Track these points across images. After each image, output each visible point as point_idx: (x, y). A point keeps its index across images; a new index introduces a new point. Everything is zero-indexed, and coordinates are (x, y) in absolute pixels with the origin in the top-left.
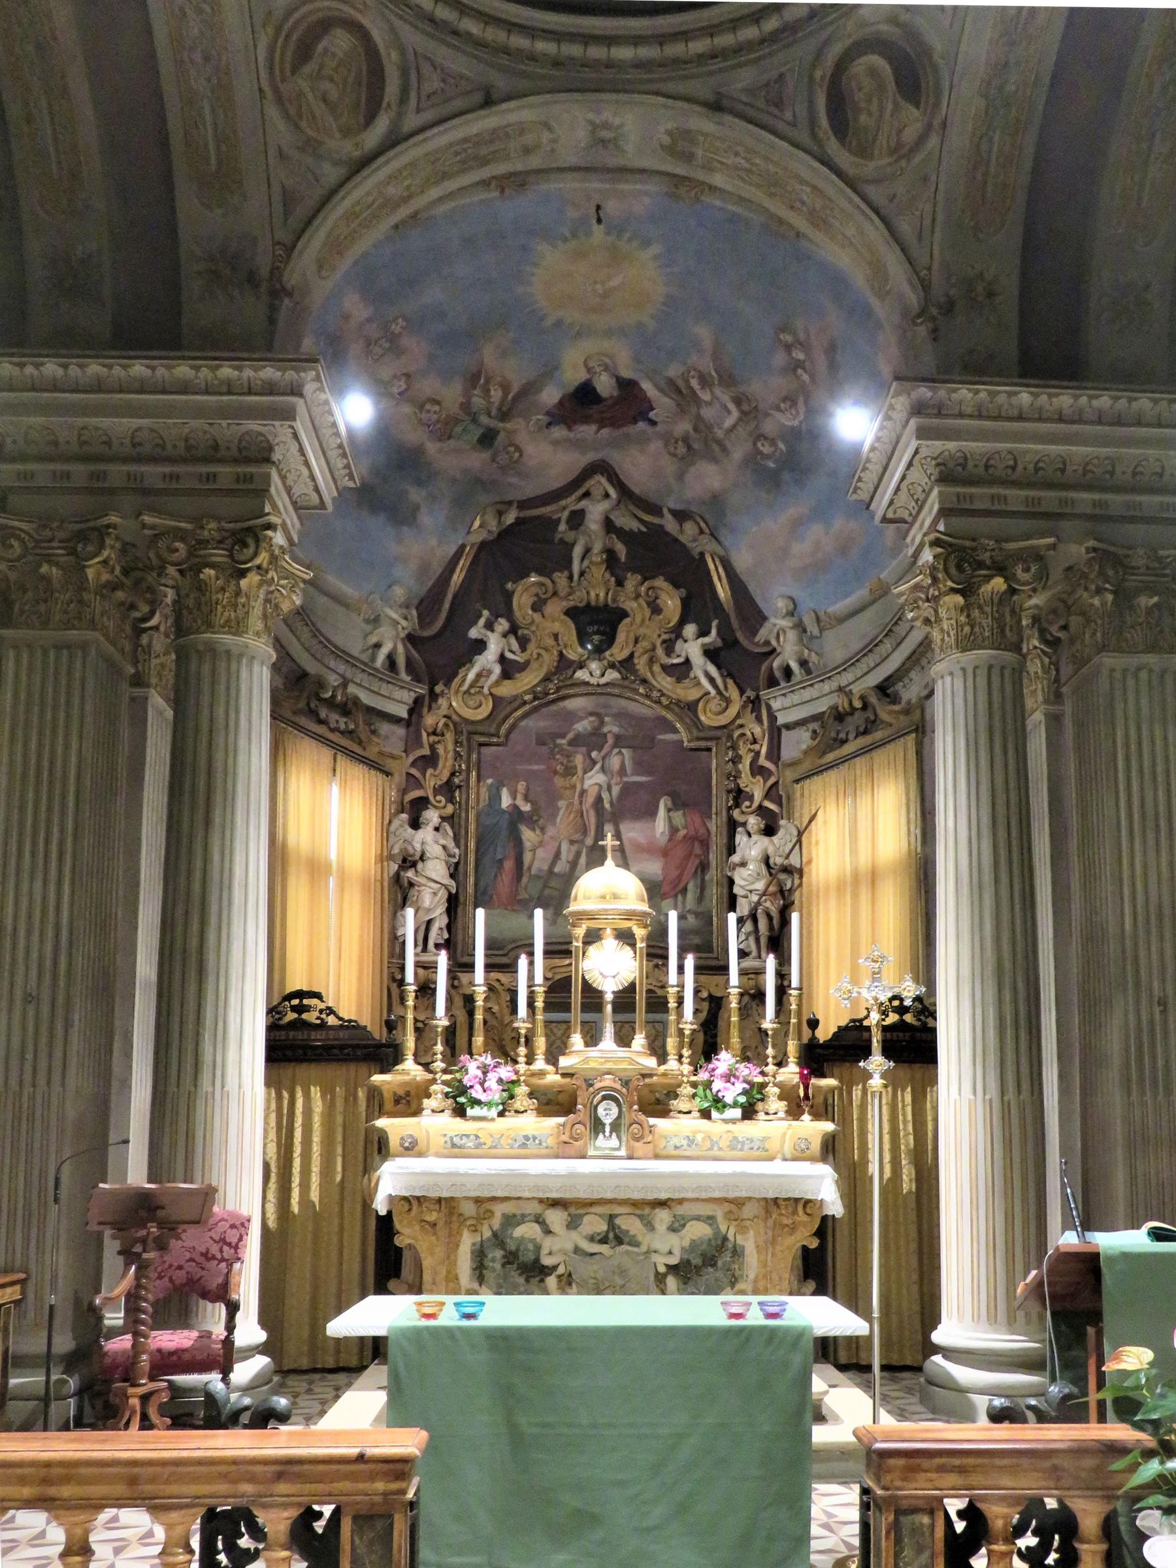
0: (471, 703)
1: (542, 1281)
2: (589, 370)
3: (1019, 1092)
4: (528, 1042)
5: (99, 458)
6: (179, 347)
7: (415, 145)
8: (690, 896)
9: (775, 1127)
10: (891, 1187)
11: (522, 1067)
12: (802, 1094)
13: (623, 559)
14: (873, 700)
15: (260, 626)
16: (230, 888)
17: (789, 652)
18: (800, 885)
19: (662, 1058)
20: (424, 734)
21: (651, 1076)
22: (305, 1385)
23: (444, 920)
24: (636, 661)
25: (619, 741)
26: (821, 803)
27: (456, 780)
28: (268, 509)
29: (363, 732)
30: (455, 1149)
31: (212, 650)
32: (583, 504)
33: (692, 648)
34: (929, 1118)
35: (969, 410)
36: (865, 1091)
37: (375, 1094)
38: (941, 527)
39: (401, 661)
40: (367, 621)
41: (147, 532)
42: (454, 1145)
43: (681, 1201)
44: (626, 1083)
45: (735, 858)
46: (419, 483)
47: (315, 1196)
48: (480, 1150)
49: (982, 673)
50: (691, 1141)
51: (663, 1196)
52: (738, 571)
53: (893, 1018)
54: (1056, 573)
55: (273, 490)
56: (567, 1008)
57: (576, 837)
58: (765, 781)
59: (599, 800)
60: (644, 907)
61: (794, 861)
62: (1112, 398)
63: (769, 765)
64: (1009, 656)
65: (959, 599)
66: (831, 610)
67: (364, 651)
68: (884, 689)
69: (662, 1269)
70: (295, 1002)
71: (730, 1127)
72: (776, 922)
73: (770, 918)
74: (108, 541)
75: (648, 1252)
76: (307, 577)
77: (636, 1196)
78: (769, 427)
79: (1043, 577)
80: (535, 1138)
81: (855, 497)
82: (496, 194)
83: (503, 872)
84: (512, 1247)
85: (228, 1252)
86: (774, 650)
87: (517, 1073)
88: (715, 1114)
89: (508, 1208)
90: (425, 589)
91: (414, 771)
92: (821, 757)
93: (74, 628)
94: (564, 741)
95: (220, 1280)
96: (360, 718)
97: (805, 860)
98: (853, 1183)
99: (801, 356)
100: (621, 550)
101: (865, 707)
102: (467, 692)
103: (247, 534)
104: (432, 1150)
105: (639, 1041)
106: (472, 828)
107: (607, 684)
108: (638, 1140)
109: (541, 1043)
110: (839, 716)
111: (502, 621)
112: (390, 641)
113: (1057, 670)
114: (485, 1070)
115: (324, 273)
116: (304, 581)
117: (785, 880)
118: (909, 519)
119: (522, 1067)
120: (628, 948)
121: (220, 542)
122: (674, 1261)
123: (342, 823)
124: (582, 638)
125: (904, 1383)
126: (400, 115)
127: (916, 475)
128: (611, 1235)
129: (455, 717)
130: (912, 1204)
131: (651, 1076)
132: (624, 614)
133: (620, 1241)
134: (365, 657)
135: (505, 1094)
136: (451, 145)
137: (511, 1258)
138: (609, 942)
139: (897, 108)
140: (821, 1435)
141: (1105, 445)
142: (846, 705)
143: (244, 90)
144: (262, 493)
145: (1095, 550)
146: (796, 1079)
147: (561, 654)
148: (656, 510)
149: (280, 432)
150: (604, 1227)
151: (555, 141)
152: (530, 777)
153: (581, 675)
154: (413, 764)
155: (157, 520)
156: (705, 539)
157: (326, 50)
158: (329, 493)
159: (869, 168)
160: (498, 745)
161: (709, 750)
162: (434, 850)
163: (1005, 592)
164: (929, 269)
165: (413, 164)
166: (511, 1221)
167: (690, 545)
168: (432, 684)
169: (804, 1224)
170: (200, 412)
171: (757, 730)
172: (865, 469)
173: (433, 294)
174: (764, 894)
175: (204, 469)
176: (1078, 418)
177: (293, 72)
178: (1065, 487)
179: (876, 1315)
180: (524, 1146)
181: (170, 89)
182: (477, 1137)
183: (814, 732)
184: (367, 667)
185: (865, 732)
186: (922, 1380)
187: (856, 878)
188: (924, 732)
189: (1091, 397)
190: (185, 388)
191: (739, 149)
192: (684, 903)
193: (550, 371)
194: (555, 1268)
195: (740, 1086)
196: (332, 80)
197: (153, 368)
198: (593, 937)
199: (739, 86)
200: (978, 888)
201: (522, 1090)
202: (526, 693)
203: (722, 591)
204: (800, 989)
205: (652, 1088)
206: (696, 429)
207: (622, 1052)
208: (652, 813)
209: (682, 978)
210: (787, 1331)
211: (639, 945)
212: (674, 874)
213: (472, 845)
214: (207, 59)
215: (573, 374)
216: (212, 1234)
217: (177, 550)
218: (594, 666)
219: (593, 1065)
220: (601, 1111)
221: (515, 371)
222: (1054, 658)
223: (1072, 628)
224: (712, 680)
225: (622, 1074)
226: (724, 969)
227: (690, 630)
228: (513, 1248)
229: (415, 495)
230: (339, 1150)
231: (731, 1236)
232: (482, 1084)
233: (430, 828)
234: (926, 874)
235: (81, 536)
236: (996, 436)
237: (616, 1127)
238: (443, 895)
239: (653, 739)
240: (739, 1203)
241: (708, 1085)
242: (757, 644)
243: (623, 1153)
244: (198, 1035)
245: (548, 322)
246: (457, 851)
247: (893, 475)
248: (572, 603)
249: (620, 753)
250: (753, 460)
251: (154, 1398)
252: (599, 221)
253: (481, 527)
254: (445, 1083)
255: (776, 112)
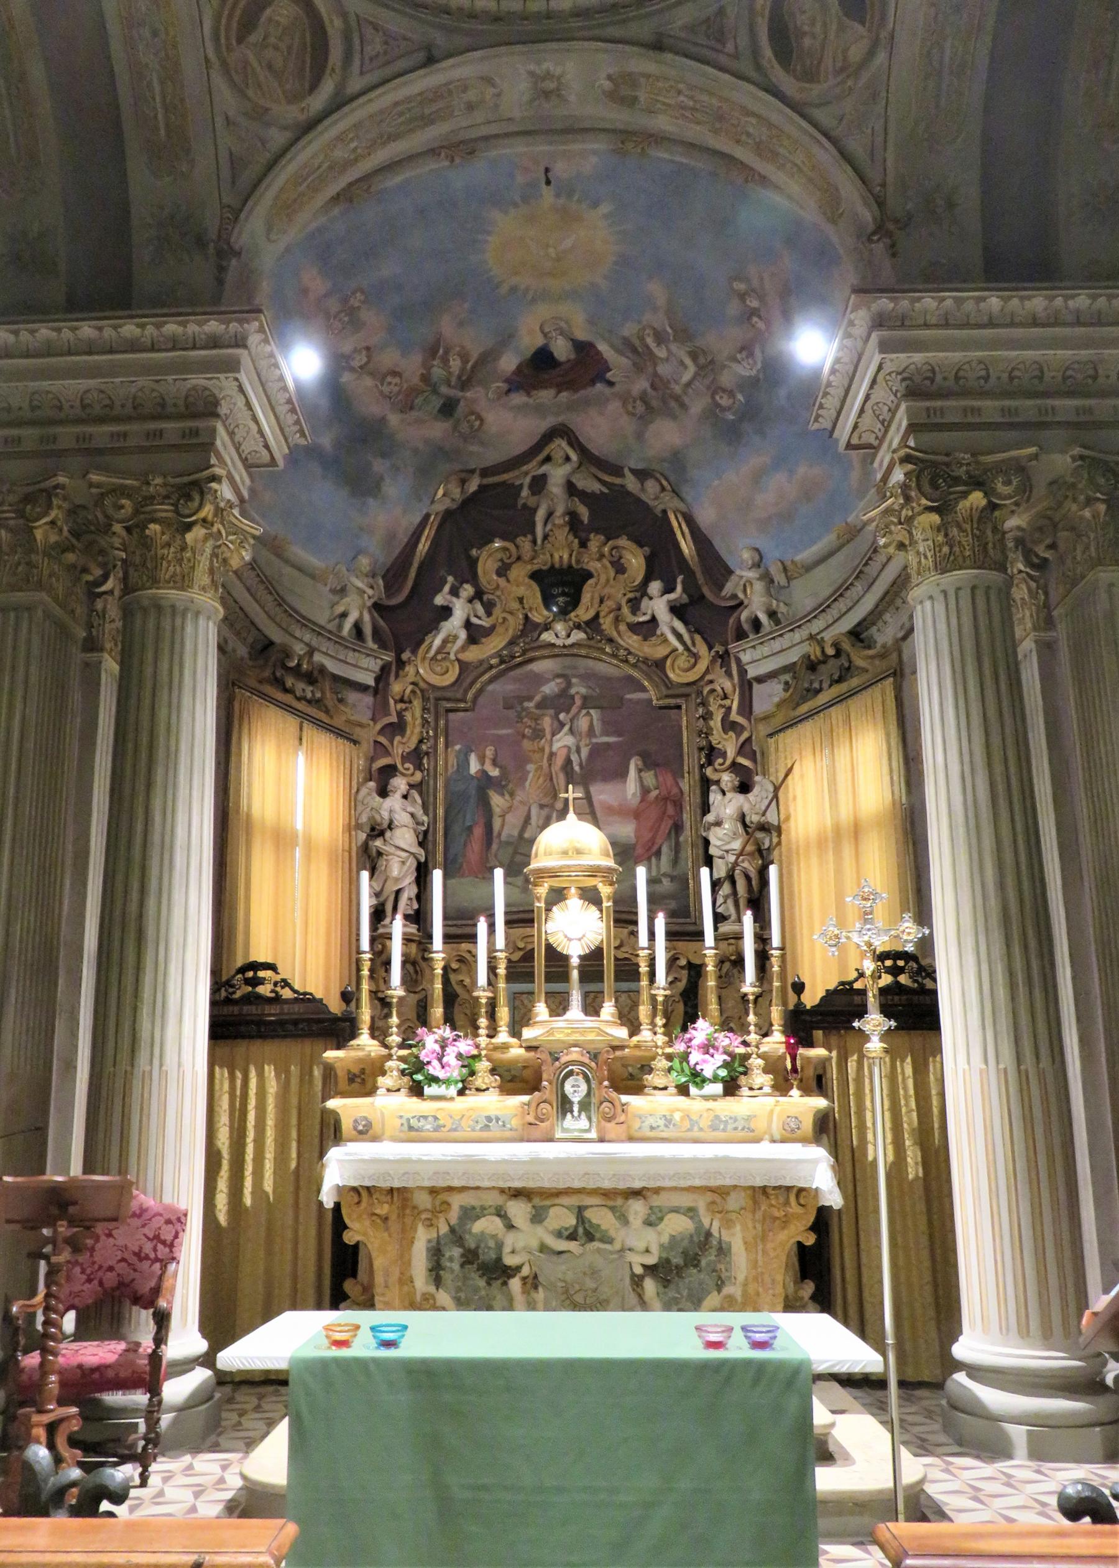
0: (438, 669)
1: (505, 1283)
2: (545, 335)
3: (1038, 1063)
4: (492, 1016)
5: (52, 422)
6: (127, 306)
7: (360, 106)
8: (664, 859)
9: (760, 1103)
10: (896, 1170)
11: (483, 1041)
12: (789, 1066)
13: (586, 521)
14: (846, 646)
15: (206, 580)
16: (172, 847)
17: (757, 604)
18: (779, 843)
19: (634, 1030)
20: (392, 702)
21: (622, 1048)
22: (254, 1401)
23: (414, 890)
24: (601, 621)
25: (587, 702)
26: (796, 757)
27: (424, 747)
28: (213, 461)
29: (330, 699)
30: (412, 1132)
31: (158, 606)
32: (545, 468)
33: (658, 606)
34: (934, 1092)
35: (934, 321)
36: (862, 1057)
37: (329, 1071)
38: (912, 443)
39: (368, 630)
40: (333, 591)
41: (94, 490)
42: (411, 1128)
43: (657, 1191)
44: (595, 1056)
45: (710, 818)
46: (384, 455)
47: (268, 1186)
48: (440, 1133)
49: (965, 594)
50: (668, 1121)
51: (637, 1185)
52: (702, 526)
53: (886, 980)
54: (1040, 489)
55: (218, 443)
56: (529, 977)
57: (545, 801)
58: (738, 736)
59: (568, 762)
60: (610, 863)
61: (772, 817)
62: (1089, 296)
63: (740, 720)
64: (994, 576)
65: (935, 518)
66: (798, 558)
67: (330, 621)
68: (857, 634)
69: (639, 1270)
70: (250, 974)
71: (711, 1104)
72: (755, 883)
73: (748, 878)
74: (55, 502)
75: (622, 1250)
76: (257, 533)
77: (607, 1184)
78: (726, 379)
79: (1026, 489)
80: (498, 1119)
81: (816, 426)
82: (447, 163)
83: (471, 835)
84: (471, 1244)
85: (162, 1251)
86: (741, 603)
87: (477, 1046)
88: (693, 1090)
89: (467, 1199)
90: (392, 559)
91: (382, 739)
92: (794, 709)
93: (20, 590)
94: (531, 704)
95: (153, 1284)
96: (327, 685)
97: (782, 817)
98: (852, 1168)
99: (755, 304)
100: (584, 512)
101: (838, 653)
102: (433, 658)
103: (194, 487)
104: (388, 1134)
105: (608, 1009)
106: (441, 795)
107: (572, 645)
108: (609, 1120)
109: (504, 1013)
110: (812, 666)
111: (467, 586)
112: (356, 609)
113: (1046, 594)
114: (443, 1044)
115: (273, 237)
116: (254, 537)
117: (763, 838)
118: (876, 443)
119: (483, 1041)
120: (593, 908)
121: (167, 497)
122: (651, 1260)
123: (308, 792)
124: (547, 601)
125: (925, 1403)
126: (344, 79)
127: (881, 394)
128: (581, 1230)
129: (422, 685)
130: (919, 1191)
131: (622, 1048)
132: (589, 575)
133: (590, 1237)
134: (331, 626)
135: (465, 1071)
136: (396, 104)
137: (470, 1257)
138: (574, 903)
139: (842, 28)
140: (827, 1480)
141: (1087, 346)
142: (819, 653)
143: (190, 65)
144: (208, 446)
145: (1082, 457)
146: (782, 1049)
147: (526, 617)
148: (617, 471)
149: (223, 385)
150: (572, 1221)
151: (499, 95)
152: (498, 741)
153: (547, 637)
154: (381, 732)
155: (103, 479)
156: (667, 497)
157: (270, 20)
158: (280, 450)
159: (815, 91)
160: (465, 710)
161: (679, 707)
162: (402, 817)
163: (984, 509)
164: (883, 185)
165: (357, 126)
166: (470, 1214)
167: (651, 503)
168: (399, 651)
169: (798, 1217)
170: (147, 369)
171: (728, 685)
172: (826, 394)
173: (388, 269)
174: (741, 854)
175: (153, 426)
176: (1054, 321)
177: (240, 40)
178: (1046, 394)
179: (890, 1341)
180: (486, 1127)
181: (120, 68)
182: (436, 1118)
183: (787, 683)
184: (335, 637)
185: (839, 680)
186: (944, 1402)
187: (837, 830)
188: (902, 675)
189: (1067, 298)
190: (133, 346)
191: (681, 86)
192: (658, 866)
193: (506, 339)
194: (518, 1268)
195: (720, 1058)
196: (276, 48)
197: (100, 329)
198: (558, 896)
199: (680, 23)
200: (975, 830)
201: (483, 1066)
202: (492, 657)
203: (686, 547)
204: (782, 949)
205: (624, 1062)
206: (653, 386)
207: (590, 1022)
208: (622, 775)
209: (653, 939)
210: (780, 1365)
211: (605, 904)
212: (647, 836)
213: (441, 812)
214: (155, 34)
215: (529, 341)
216: (146, 1230)
217: (122, 507)
218: (559, 627)
219: (559, 1036)
220: (568, 1088)
221: (473, 341)
222: (1042, 581)
223: (1062, 546)
224: (679, 636)
225: (590, 1047)
226: (699, 935)
227: (655, 587)
228: (473, 1246)
229: (379, 466)
230: (294, 1134)
231: (715, 1233)
232: (440, 1060)
233: (398, 796)
234: (912, 823)
235: (28, 499)
236: (964, 345)
237: (585, 1106)
238: (412, 864)
239: (622, 699)
240: (722, 1192)
241: (685, 1057)
242: (724, 599)
243: (593, 1135)
244: (135, 1009)
245: (504, 289)
246: (425, 818)
247: (855, 398)
248: (536, 567)
249: (588, 713)
250: (713, 413)
251: (64, 1426)
252: (548, 182)
253: (445, 496)
254: (402, 1059)
255: (719, 46)
